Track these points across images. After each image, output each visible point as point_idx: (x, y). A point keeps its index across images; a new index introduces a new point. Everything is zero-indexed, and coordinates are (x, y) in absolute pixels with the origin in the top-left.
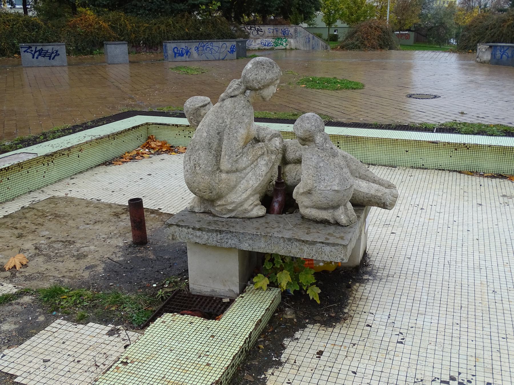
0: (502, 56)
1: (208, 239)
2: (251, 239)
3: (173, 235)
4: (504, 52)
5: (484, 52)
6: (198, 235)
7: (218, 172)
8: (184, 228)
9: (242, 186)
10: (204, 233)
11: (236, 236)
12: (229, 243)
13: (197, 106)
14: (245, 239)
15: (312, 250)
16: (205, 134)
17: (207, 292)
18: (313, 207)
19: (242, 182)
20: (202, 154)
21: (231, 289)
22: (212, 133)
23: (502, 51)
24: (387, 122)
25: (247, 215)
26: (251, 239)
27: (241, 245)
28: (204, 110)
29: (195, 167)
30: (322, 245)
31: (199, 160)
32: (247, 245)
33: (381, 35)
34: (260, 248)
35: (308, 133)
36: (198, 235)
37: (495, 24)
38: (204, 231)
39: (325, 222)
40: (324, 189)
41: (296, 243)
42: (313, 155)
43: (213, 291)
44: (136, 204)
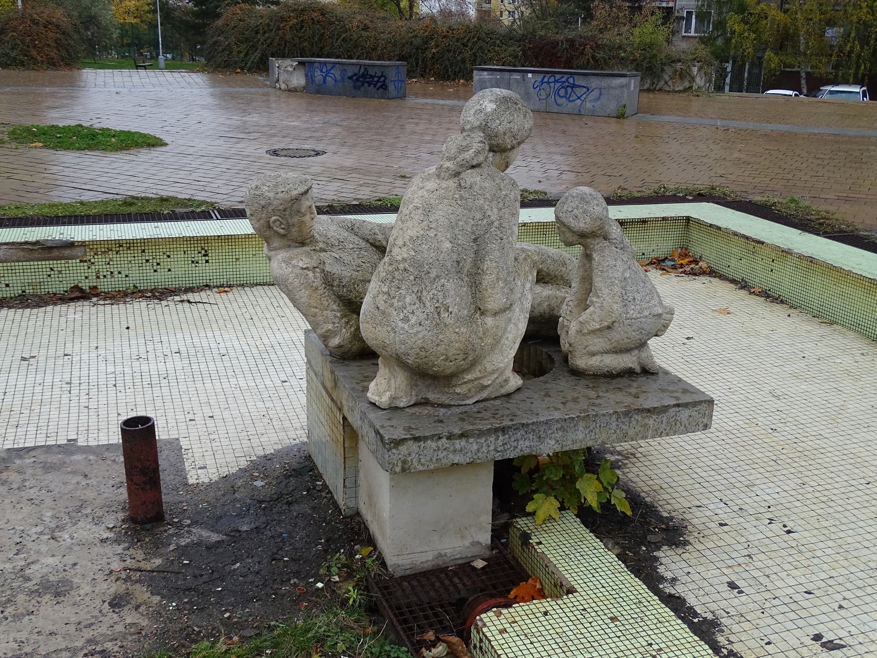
0: (324, 79)
1: (478, 450)
2: (560, 429)
3: (404, 462)
4: (328, 72)
5: (291, 73)
6: (458, 447)
7: (477, 315)
8: (429, 442)
9: (510, 336)
10: (471, 440)
11: (534, 431)
12: (519, 447)
13: (296, 192)
14: (550, 432)
15: (662, 422)
16: (448, 245)
17: (427, 561)
18: (607, 352)
19: (509, 329)
20: (448, 285)
21: (476, 540)
22: (462, 240)
23: (324, 70)
24: (648, 192)
25: (503, 391)
26: (560, 429)
27: (541, 447)
28: (308, 199)
29: (439, 313)
30: (677, 409)
31: (444, 297)
32: (553, 442)
33: (60, 40)
34: (574, 442)
35: (598, 223)
36: (458, 447)
37: (268, 25)
38: (472, 436)
39: (629, 373)
40: (638, 316)
41: (636, 417)
42: (616, 260)
43: (440, 555)
44: (139, 433)
